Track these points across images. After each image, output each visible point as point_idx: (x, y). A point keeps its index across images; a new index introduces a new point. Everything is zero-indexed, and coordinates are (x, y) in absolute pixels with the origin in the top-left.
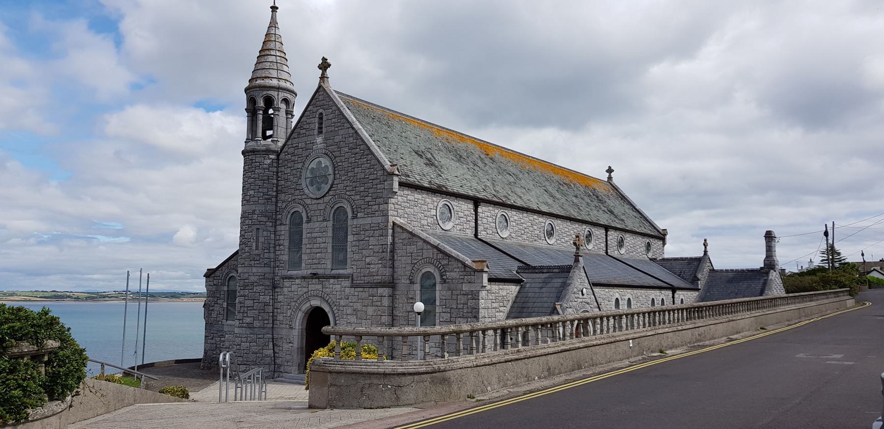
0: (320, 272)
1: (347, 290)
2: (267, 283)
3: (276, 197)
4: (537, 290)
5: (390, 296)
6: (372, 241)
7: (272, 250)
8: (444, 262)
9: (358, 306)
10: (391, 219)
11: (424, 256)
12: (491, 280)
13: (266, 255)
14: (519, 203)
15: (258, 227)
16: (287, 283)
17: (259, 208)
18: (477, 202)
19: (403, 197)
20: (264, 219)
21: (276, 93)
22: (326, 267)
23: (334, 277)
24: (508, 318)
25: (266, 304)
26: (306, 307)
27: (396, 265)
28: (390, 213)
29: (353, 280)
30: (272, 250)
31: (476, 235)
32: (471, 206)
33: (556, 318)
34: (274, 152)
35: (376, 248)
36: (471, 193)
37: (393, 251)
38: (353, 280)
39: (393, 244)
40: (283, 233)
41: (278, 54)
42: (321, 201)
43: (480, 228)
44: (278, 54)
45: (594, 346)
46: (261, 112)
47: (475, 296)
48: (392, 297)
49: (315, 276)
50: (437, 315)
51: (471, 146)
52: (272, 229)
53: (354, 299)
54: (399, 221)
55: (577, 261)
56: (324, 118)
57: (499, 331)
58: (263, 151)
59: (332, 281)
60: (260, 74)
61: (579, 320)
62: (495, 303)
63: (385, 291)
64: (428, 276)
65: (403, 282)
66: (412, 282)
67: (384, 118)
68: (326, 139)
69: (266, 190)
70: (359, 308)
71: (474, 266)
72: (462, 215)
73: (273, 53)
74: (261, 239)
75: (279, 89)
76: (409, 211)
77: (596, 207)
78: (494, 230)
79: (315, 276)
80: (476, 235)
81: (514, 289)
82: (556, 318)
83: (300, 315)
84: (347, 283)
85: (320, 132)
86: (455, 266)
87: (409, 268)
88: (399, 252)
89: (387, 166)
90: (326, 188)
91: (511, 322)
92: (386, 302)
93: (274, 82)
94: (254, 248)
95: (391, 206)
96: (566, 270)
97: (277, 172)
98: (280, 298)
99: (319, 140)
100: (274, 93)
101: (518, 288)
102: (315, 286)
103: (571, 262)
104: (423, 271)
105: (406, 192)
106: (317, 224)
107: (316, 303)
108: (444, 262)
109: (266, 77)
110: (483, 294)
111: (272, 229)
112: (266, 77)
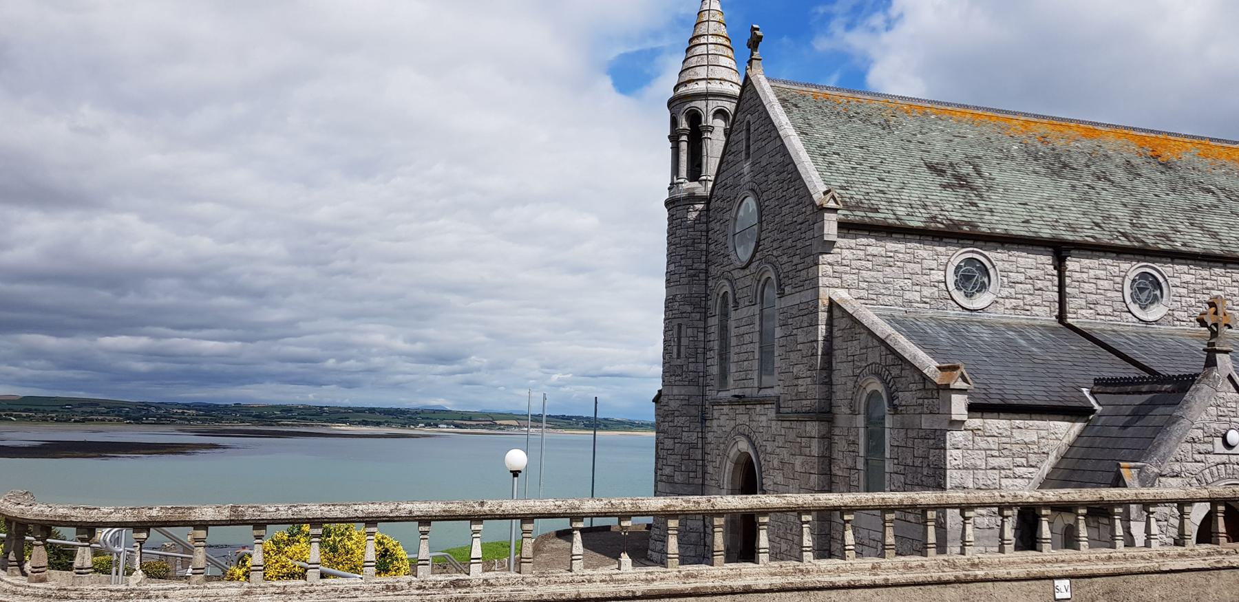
0: (748, 392)
2: (693, 411)
3: (707, 271)
4: (1115, 432)
5: (823, 437)
6: (801, 339)
7: (700, 357)
8: (895, 371)
10: (825, 294)
11: (870, 361)
12: (973, 409)
13: (692, 367)
14: (1202, 243)
15: (680, 321)
17: (684, 291)
18: (1060, 250)
19: (849, 250)
20: (689, 309)
21: (704, 103)
24: (1046, 483)
25: (693, 446)
26: (733, 453)
27: (834, 379)
28: (822, 281)
29: (779, 407)
30: (700, 357)
31: (1061, 317)
32: (1046, 260)
33: (927, 497)
34: (701, 199)
36: (1046, 233)
37: (829, 352)
38: (779, 407)
39: (829, 338)
41: (711, 40)
42: (747, 272)
43: (1071, 305)
44: (711, 40)
45: (995, 580)
46: (684, 138)
47: (937, 440)
48: (827, 439)
50: (887, 476)
51: (1111, 144)
52: (701, 324)
54: (841, 295)
55: (1211, 363)
56: (752, 129)
57: (1012, 514)
58: (684, 199)
60: (689, 75)
61: (1214, 502)
62: (997, 460)
63: (813, 428)
64: (874, 395)
65: (842, 411)
66: (854, 413)
68: (753, 164)
69: (690, 262)
71: (938, 378)
72: (1021, 278)
73: (703, 40)
74: (684, 341)
75: (706, 96)
76: (854, 278)
77: (876, 210)
78: (1118, 306)
80: (1061, 317)
81: (1065, 431)
82: (927, 497)
83: (729, 466)
85: (748, 155)
86: (911, 379)
87: (850, 384)
88: (839, 355)
89: (818, 197)
91: (1051, 495)
92: (815, 448)
93: (701, 87)
94: (675, 356)
95: (822, 269)
96: (1184, 384)
97: (708, 232)
99: (746, 167)
100: (700, 104)
103: (1197, 366)
104: (869, 390)
105: (864, 241)
108: (895, 371)
109: (690, 81)
110: (954, 437)
111: (701, 324)
112: (690, 81)
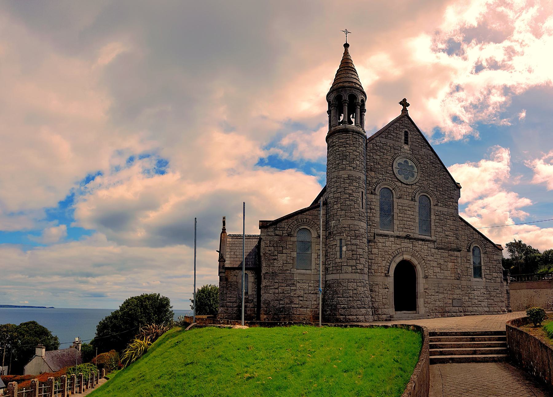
0: (412, 235)
1: (433, 250)
9: (442, 262)
16: (381, 239)
22: (416, 233)
23: (423, 240)
26: (398, 260)
35: (452, 227)
40: (374, 200)
42: (410, 187)
49: (408, 237)
53: (438, 257)
59: (420, 242)
67: (438, 133)
70: (442, 263)
79: (408, 237)
84: (431, 245)
85: (406, 142)
90: (396, 171)
98: (375, 251)
101: (505, 154)
102: (406, 244)
106: (407, 202)
107: (407, 257)
108: (485, 242)
